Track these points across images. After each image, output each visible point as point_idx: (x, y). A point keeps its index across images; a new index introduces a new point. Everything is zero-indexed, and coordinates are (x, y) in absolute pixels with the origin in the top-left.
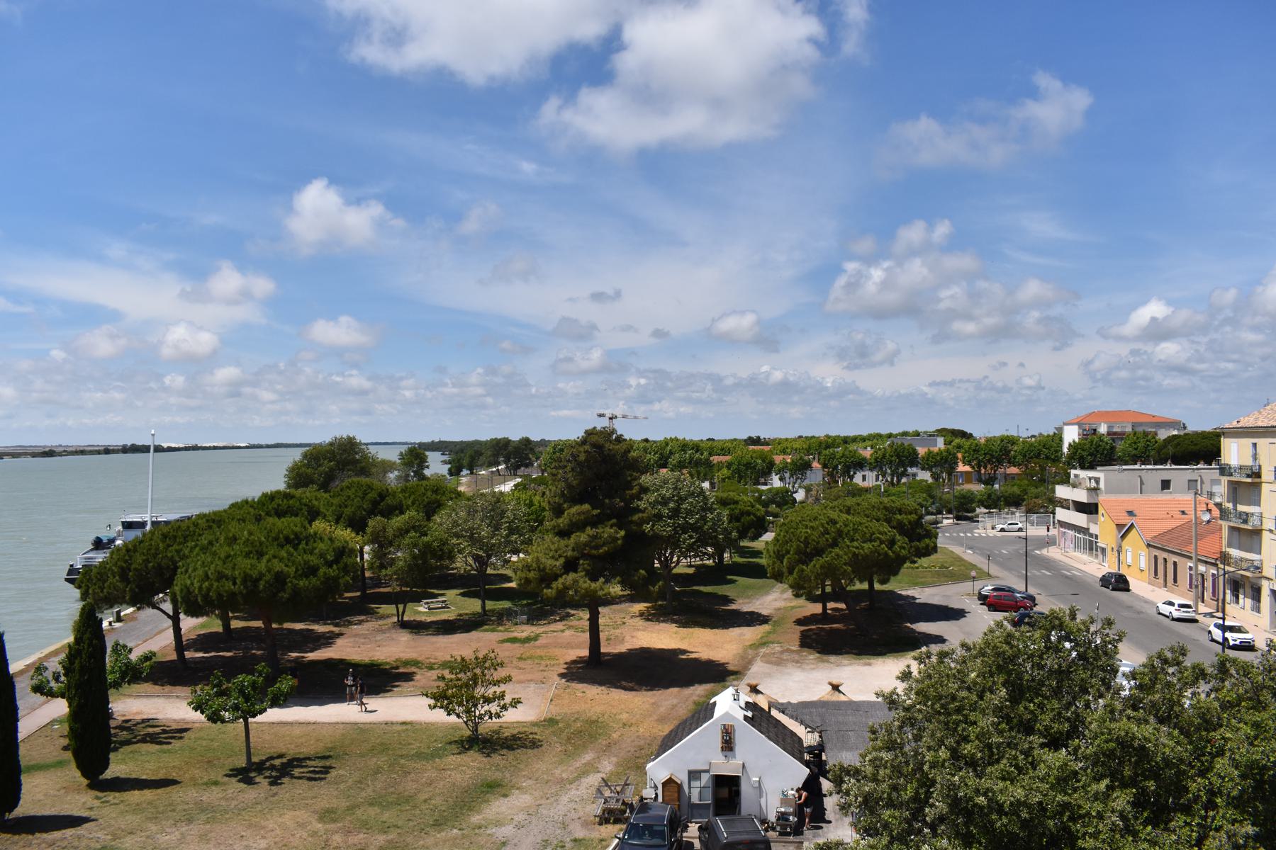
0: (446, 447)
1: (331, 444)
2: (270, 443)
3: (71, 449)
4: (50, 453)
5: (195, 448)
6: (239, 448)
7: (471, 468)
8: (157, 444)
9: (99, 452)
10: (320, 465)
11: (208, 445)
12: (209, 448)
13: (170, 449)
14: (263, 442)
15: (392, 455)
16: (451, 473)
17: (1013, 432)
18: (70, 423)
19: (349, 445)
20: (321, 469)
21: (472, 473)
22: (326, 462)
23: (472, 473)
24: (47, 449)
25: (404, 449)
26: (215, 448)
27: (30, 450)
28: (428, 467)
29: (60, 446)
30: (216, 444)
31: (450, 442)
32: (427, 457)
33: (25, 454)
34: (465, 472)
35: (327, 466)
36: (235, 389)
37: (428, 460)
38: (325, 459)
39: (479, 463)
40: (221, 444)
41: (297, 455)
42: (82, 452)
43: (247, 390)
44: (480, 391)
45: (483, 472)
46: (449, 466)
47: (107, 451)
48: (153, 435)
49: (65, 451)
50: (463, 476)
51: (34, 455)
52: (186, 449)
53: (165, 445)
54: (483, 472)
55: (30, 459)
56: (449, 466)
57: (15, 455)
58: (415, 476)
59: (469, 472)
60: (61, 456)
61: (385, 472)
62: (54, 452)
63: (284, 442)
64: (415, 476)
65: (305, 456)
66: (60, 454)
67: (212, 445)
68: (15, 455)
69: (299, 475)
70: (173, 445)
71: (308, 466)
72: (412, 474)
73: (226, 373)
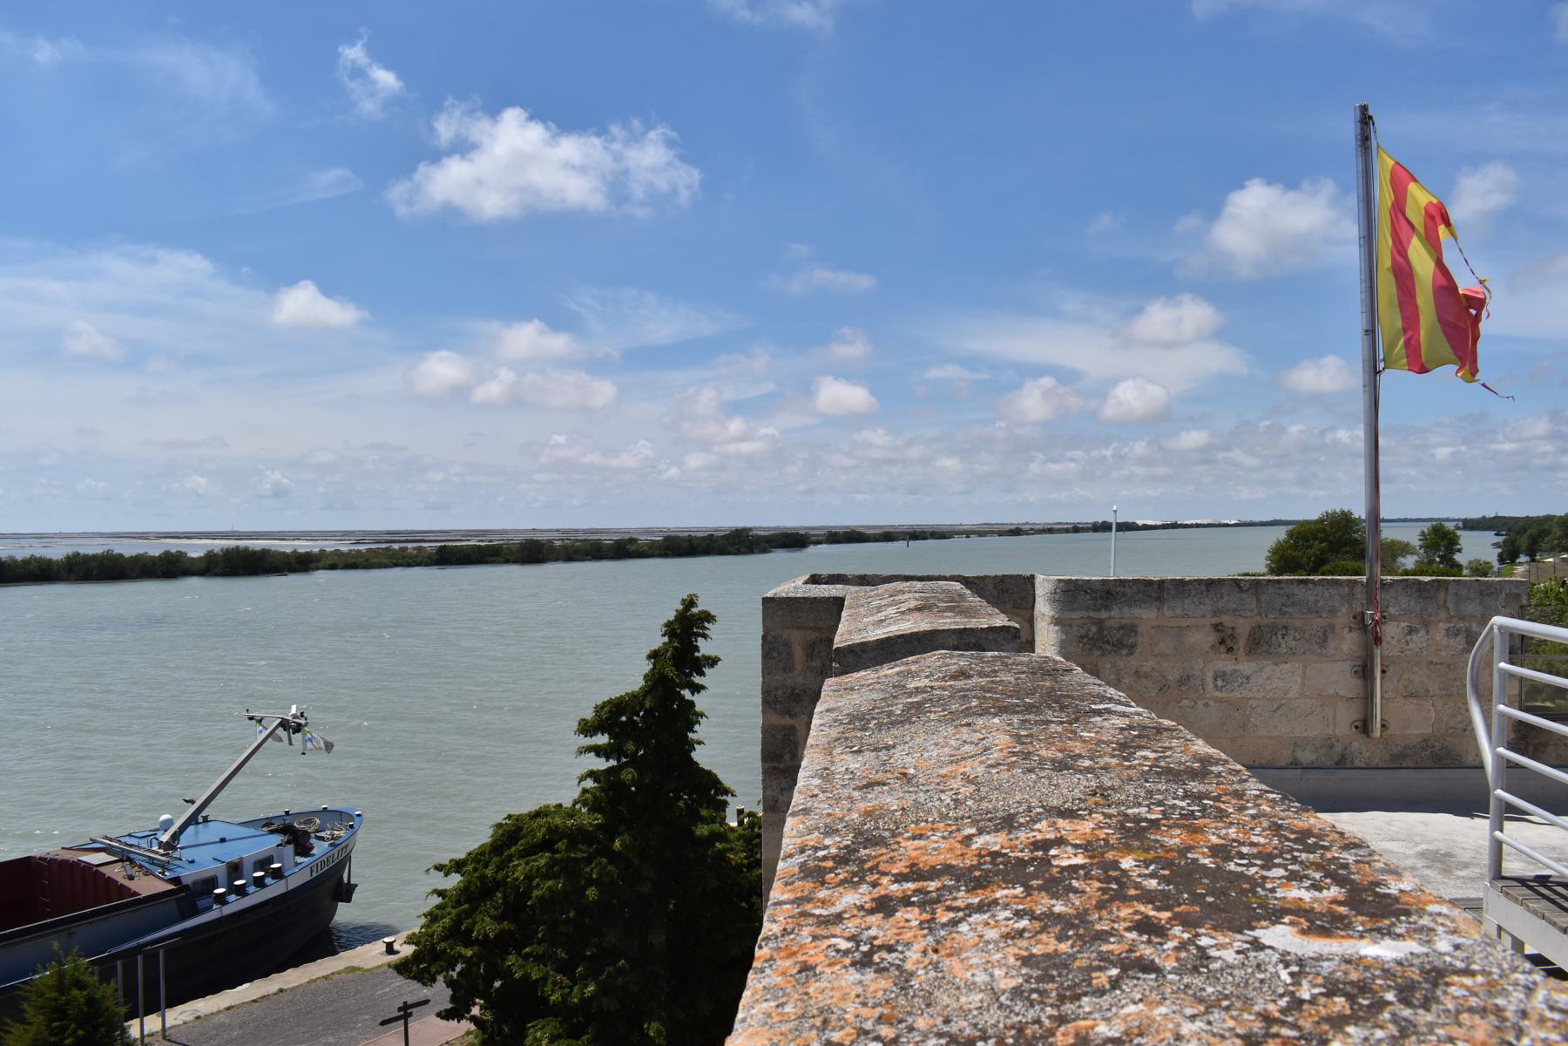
0: (1504, 525)
1: (1321, 521)
2: (1264, 520)
3: (1039, 527)
4: (1016, 532)
5: (1175, 526)
6: (1227, 525)
7: (1531, 554)
8: (1120, 521)
9: (1067, 531)
10: (1308, 547)
11: (1189, 522)
12: (1191, 526)
13: (1146, 527)
14: (1257, 519)
15: (1412, 536)
16: (1501, 559)
17: (1552, 513)
18: (1032, 499)
19: (1344, 522)
20: (1311, 551)
21: (1533, 560)
22: (1316, 542)
23: (1533, 560)
24: (1013, 527)
25: (1426, 527)
26: (1198, 526)
27: (996, 528)
28: (1459, 551)
29: (1027, 523)
30: (1199, 522)
31: (1510, 518)
32: (1458, 537)
33: (992, 533)
34: (1523, 558)
35: (1318, 547)
36: (1205, 456)
37: (1460, 542)
38: (1315, 539)
39: (1544, 546)
40: (1205, 522)
41: (1281, 534)
42: (1050, 531)
43: (1221, 455)
44: (1548, 447)
45: (1551, 560)
46: (1500, 550)
47: (1076, 529)
48: (1115, 511)
49: (1032, 529)
50: (1520, 564)
51: (1001, 533)
52: (1164, 527)
53: (1140, 523)
54: (1551, 560)
55: (996, 538)
56: (1500, 550)
57: (981, 534)
58: (1441, 562)
59: (1527, 559)
60: (1028, 534)
61: (1394, 557)
62: (1021, 530)
63: (931, 573)
64: (1441, 562)
65: (1291, 534)
66: (1027, 533)
67: (1194, 522)
68: (981, 534)
69: (1283, 558)
70: (1150, 522)
71: (1295, 547)
72: (1438, 559)
73: (1193, 439)
